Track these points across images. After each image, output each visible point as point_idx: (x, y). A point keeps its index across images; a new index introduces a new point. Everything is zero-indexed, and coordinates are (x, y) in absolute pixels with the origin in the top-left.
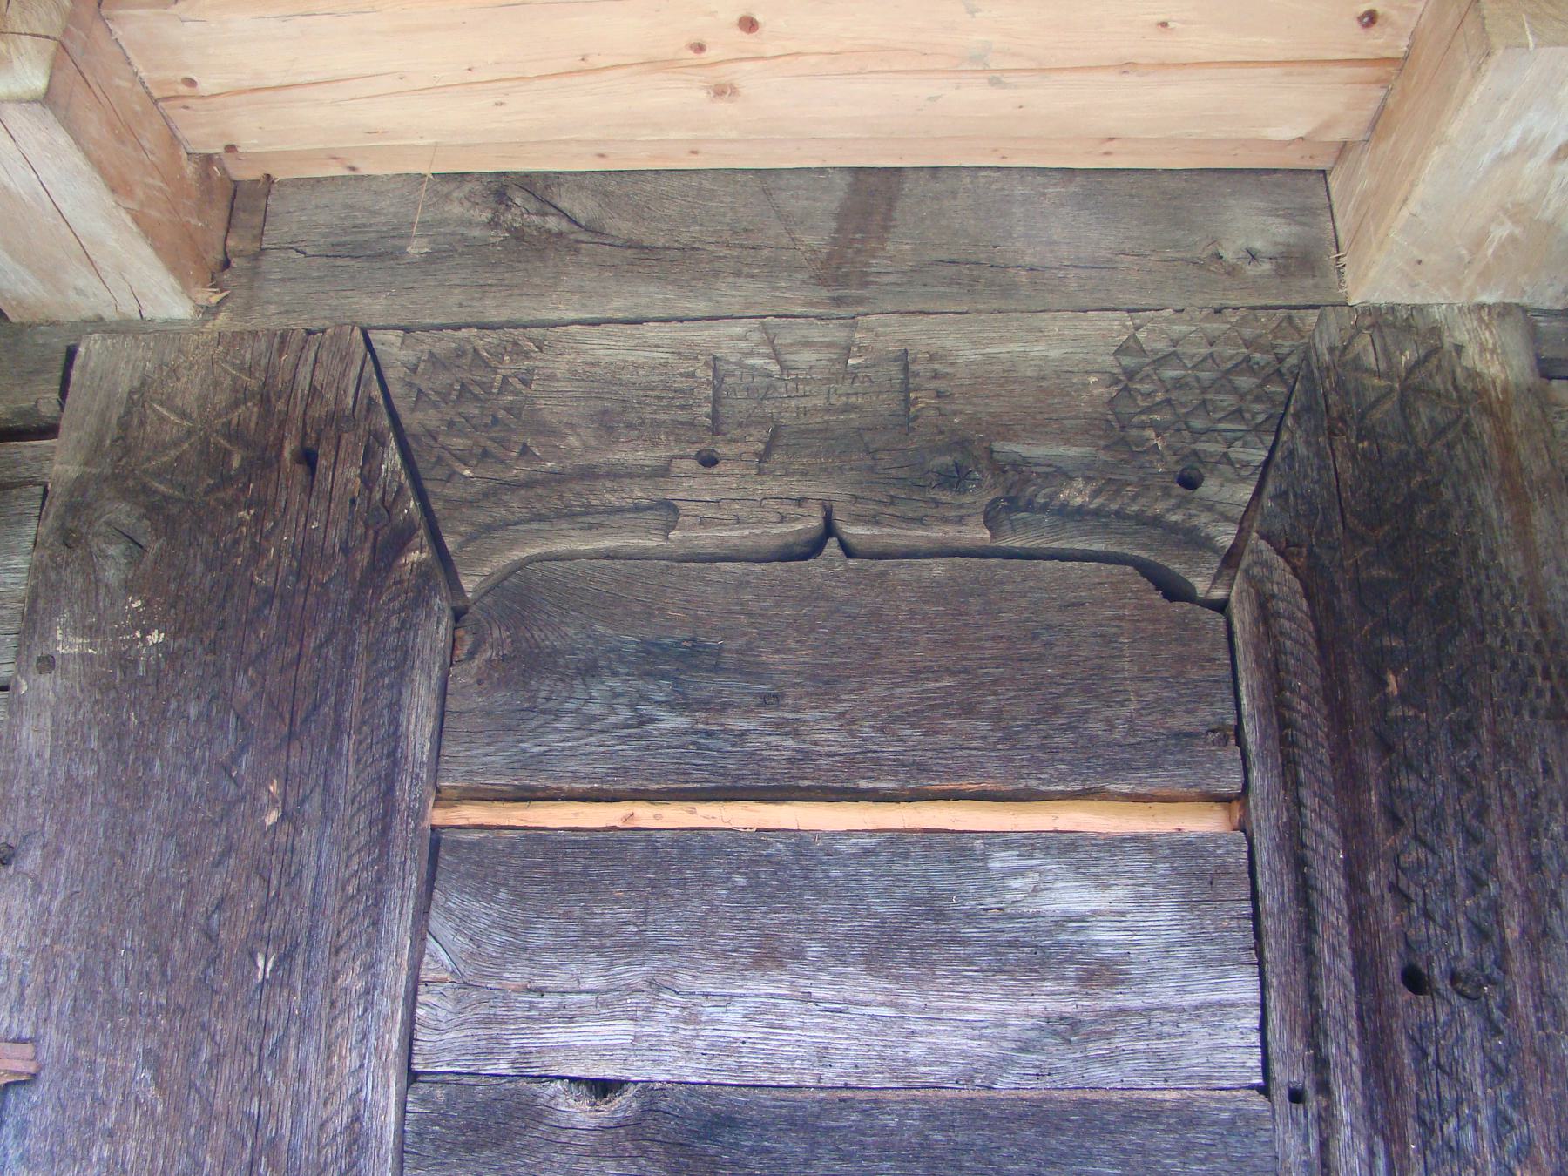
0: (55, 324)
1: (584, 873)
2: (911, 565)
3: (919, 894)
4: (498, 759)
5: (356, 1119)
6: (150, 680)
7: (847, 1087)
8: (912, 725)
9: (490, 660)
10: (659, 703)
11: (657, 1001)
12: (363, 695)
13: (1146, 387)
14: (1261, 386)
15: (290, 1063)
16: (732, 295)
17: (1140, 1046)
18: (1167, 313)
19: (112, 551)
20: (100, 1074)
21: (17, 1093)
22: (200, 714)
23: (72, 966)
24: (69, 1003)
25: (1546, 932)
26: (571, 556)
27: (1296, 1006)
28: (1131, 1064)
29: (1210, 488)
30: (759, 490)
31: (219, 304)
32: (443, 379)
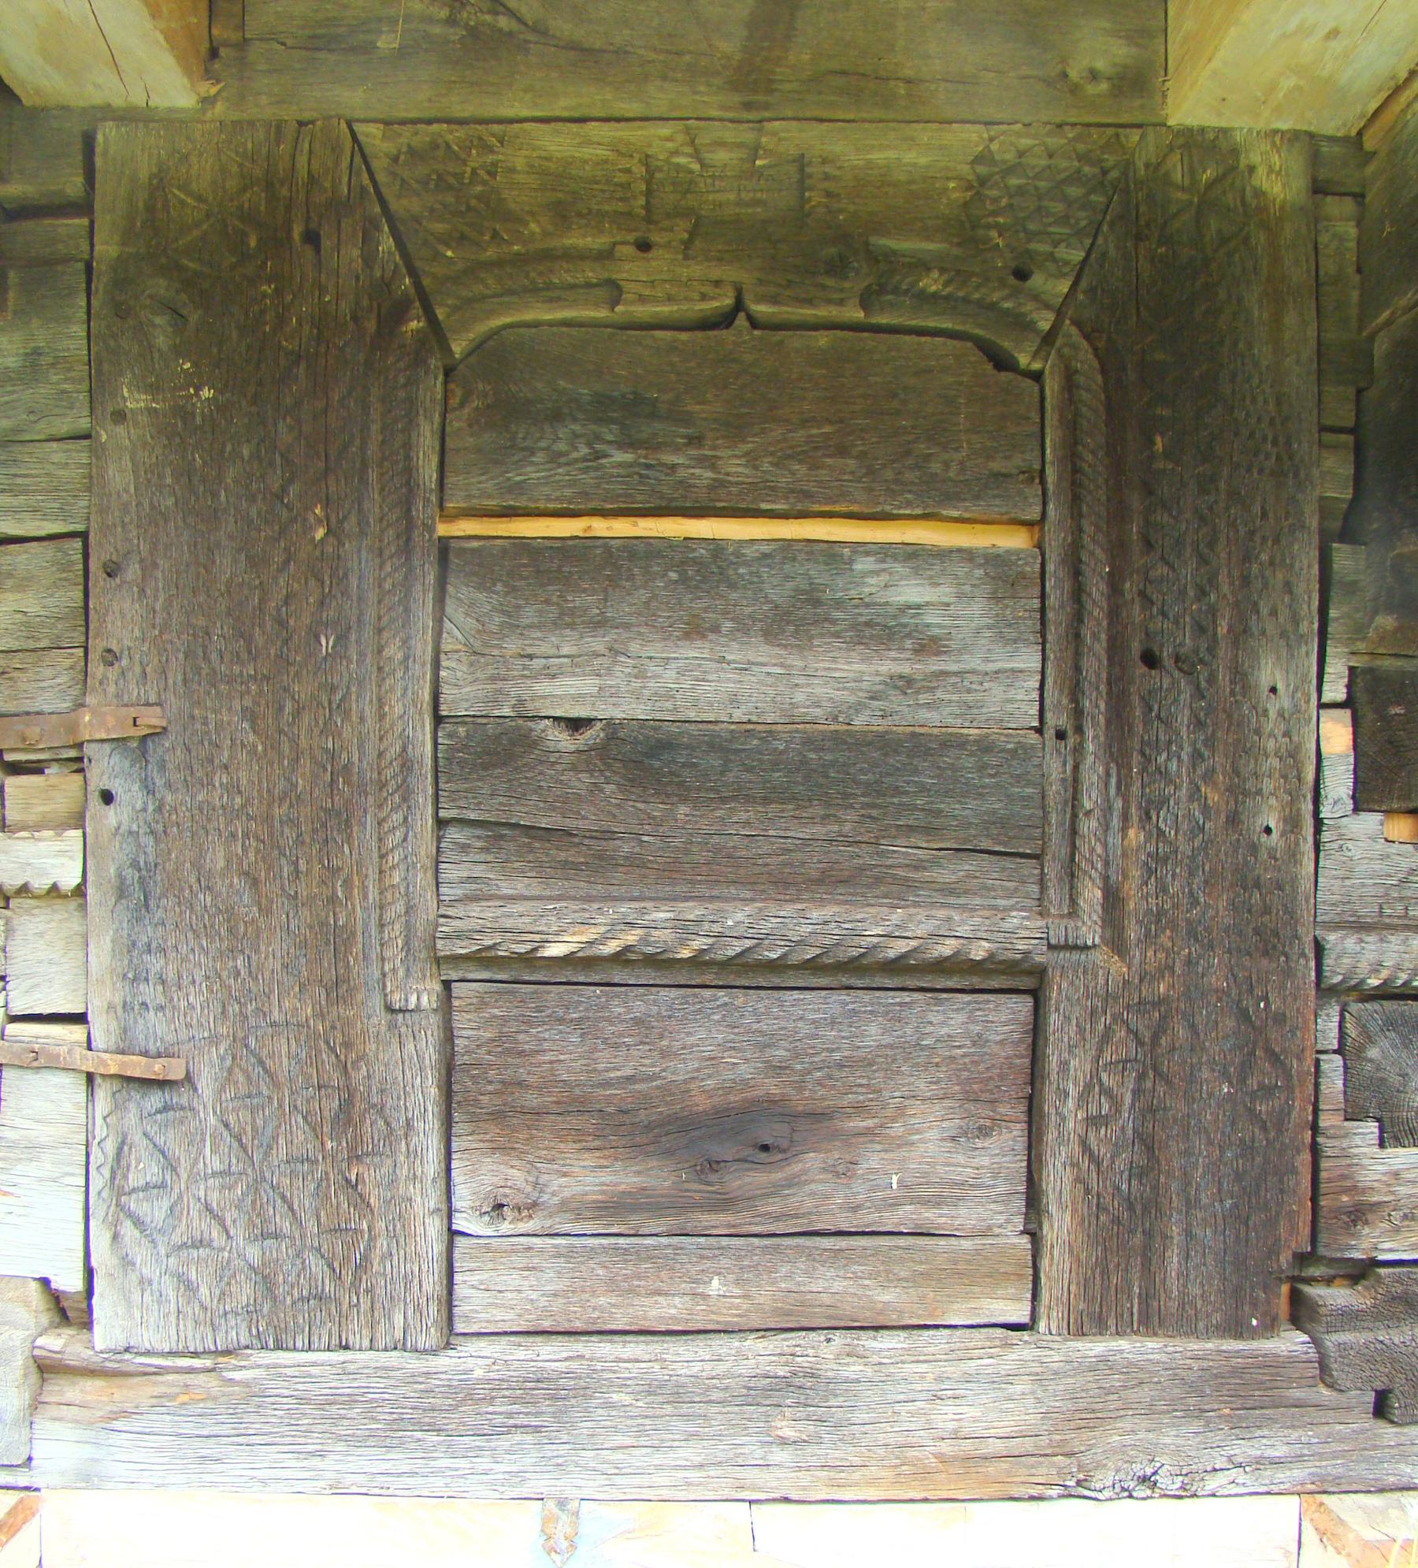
0: (66, 108)
1: (559, 570)
3: (802, 587)
5: (404, 749)
7: (750, 722)
8: (801, 462)
9: (477, 408)
10: (610, 443)
11: (615, 662)
12: (380, 438)
13: (994, 193)
16: (660, 98)
17: (955, 697)
20: (212, 726)
24: (180, 678)
26: (536, 324)
29: (1037, 281)
30: (684, 272)
32: (421, 170)
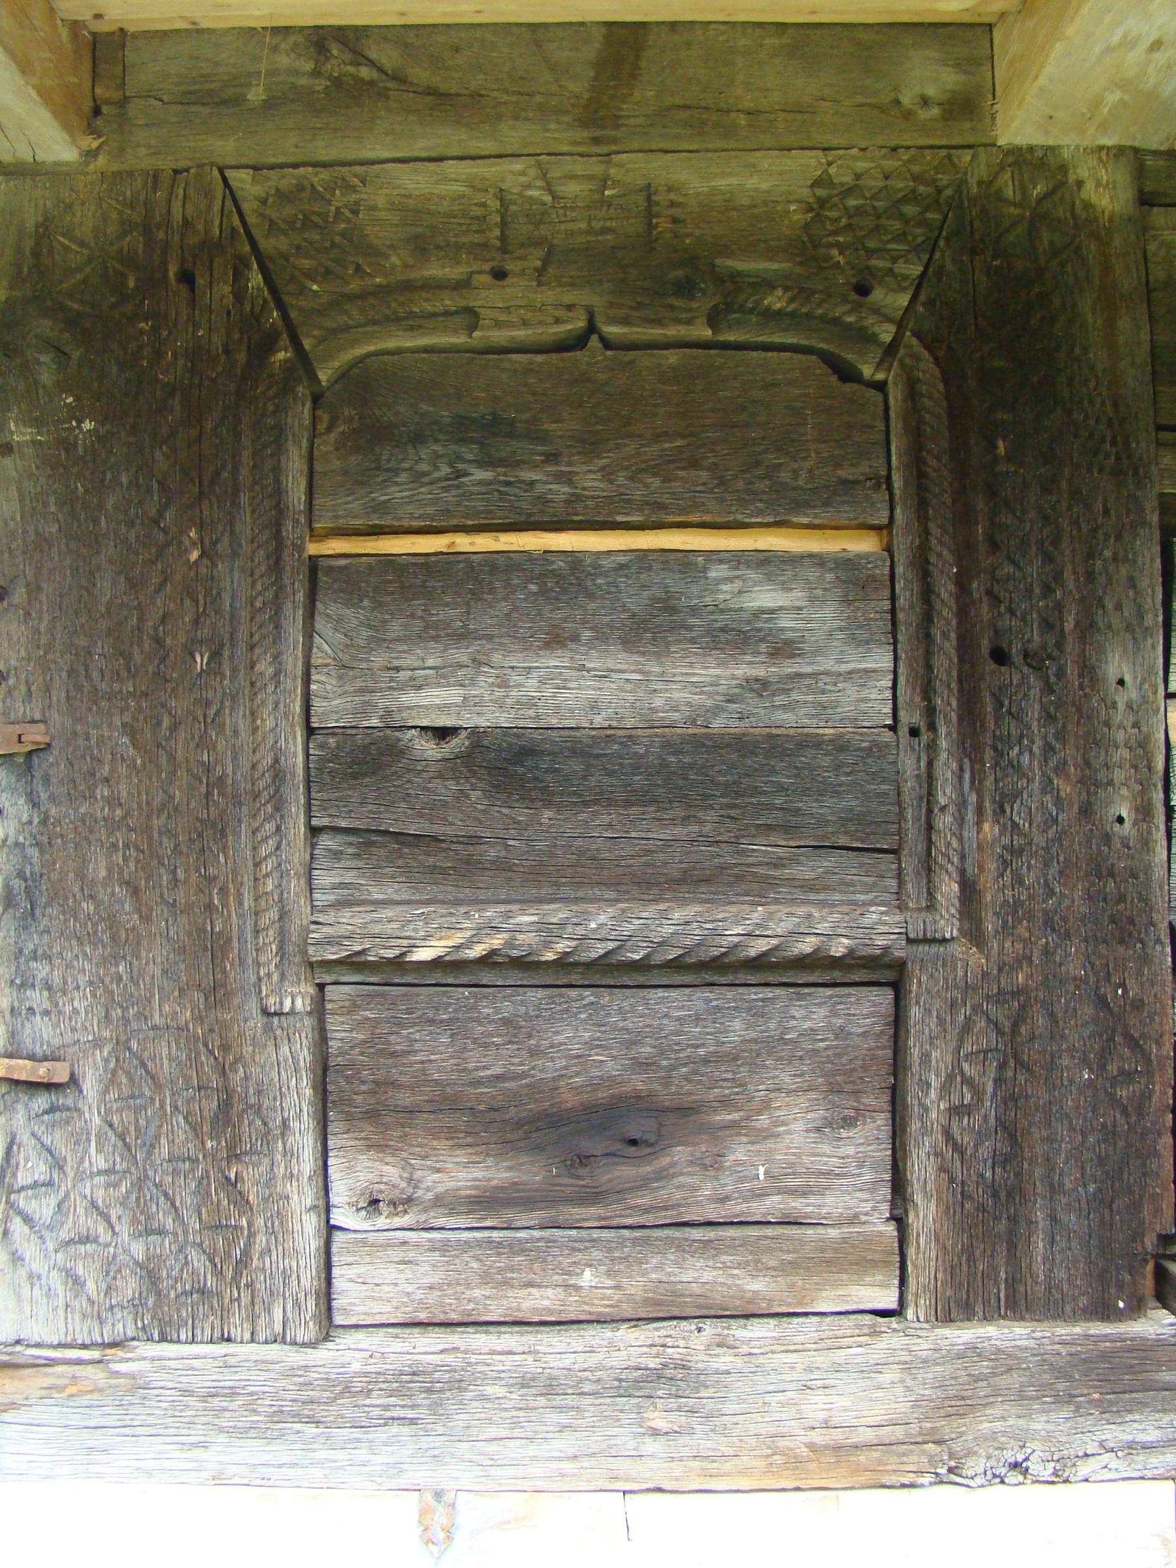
2: (653, 355)
4: (356, 506)
5: (276, 761)
6: (88, 458)
7: (610, 727)
8: (654, 475)
9: (343, 433)
10: (470, 462)
11: (478, 673)
13: (834, 214)
14: (922, 213)
15: (227, 726)
16: (513, 135)
17: (810, 698)
18: (854, 151)
19: (43, 358)
21: (39, 757)
22: (130, 483)
23: (61, 669)
24: (63, 695)
25: (1092, 625)
26: (398, 352)
27: (917, 673)
28: (802, 711)
29: (878, 295)
30: (539, 298)
31: (99, 148)
32: (288, 210)
